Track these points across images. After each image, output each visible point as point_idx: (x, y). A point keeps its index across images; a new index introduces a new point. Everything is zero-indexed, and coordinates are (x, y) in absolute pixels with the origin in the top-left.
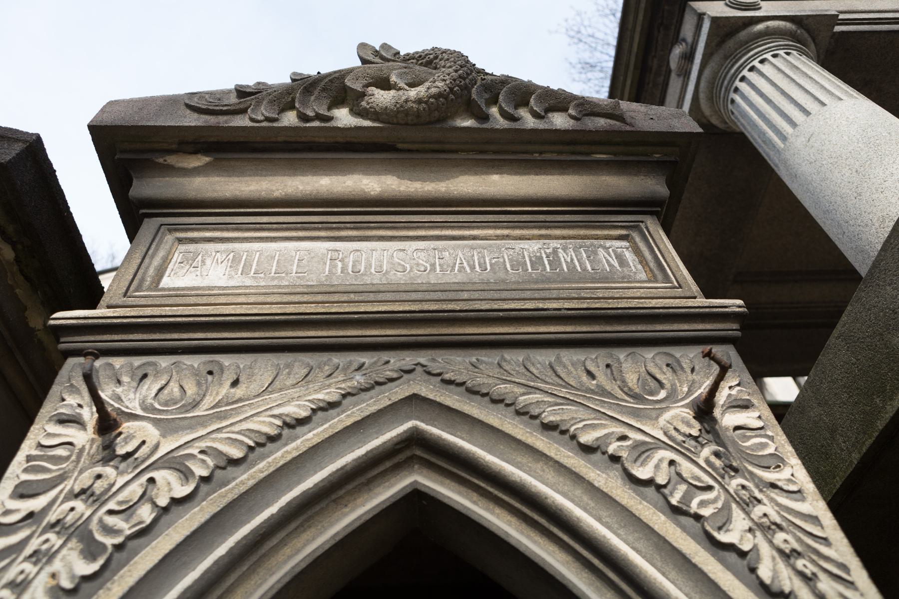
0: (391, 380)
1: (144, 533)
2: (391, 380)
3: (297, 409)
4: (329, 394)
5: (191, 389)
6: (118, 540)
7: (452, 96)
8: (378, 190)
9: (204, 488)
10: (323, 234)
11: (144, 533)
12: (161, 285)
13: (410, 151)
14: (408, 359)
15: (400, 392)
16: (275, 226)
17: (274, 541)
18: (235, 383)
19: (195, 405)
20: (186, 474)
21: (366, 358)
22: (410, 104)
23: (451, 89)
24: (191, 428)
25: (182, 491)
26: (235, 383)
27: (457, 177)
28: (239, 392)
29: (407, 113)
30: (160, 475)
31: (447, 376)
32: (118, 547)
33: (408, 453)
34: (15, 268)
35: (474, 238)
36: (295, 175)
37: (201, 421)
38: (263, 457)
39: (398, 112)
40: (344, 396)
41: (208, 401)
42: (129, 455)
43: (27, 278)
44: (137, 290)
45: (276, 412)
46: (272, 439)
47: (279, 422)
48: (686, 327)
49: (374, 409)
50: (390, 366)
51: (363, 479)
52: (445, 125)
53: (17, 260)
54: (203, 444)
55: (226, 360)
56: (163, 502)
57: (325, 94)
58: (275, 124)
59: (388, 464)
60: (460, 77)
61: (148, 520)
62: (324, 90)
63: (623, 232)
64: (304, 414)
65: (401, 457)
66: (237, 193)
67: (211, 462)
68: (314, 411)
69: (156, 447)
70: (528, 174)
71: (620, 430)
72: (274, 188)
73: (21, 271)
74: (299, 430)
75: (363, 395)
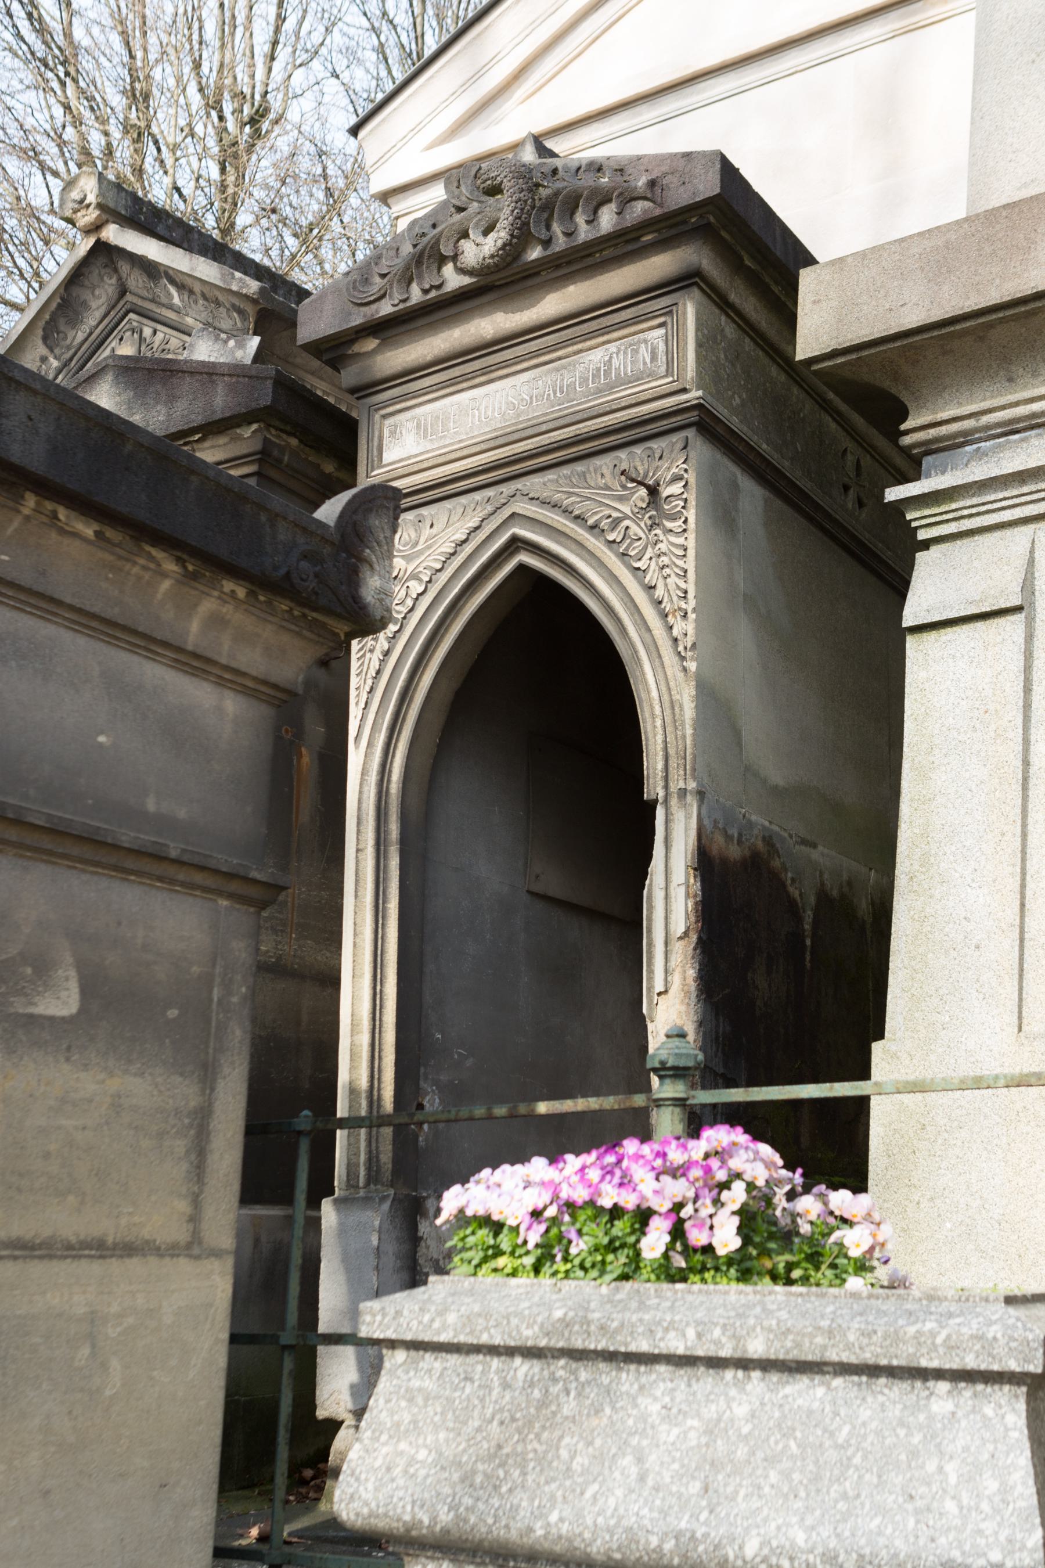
0: (504, 504)
1: (411, 610)
2: (504, 504)
3: (461, 536)
4: (473, 523)
5: (413, 535)
6: (403, 615)
7: (515, 240)
8: (492, 332)
9: (429, 585)
10: (465, 385)
11: (411, 610)
12: (384, 462)
13: (507, 284)
14: (507, 489)
15: (506, 512)
16: (434, 388)
17: (462, 602)
18: (432, 526)
19: (417, 543)
20: (420, 580)
21: (490, 492)
22: (488, 261)
23: (512, 235)
24: (418, 556)
25: (421, 589)
26: (432, 526)
27: (544, 298)
28: (434, 531)
29: (488, 266)
30: (411, 583)
31: (530, 496)
32: (404, 618)
33: (515, 546)
34: (302, 446)
35: (560, 359)
36: (436, 334)
37: (421, 552)
38: (450, 564)
39: (482, 269)
40: (482, 521)
41: (422, 540)
42: (396, 577)
43: (310, 447)
44: (372, 471)
45: (452, 539)
46: (453, 554)
47: (454, 545)
48: (665, 422)
49: (495, 527)
50: (503, 495)
51: (495, 565)
52: (520, 263)
53: (301, 441)
54: (424, 565)
55: (424, 511)
56: (415, 596)
57: (432, 260)
58: (408, 304)
59: (506, 554)
60: (516, 218)
61: (411, 605)
62: (429, 257)
63: (661, 320)
64: (464, 537)
65: (512, 549)
66: (405, 365)
67: (429, 573)
68: (469, 534)
69: (406, 570)
70: (595, 276)
71: (607, 512)
72: (426, 352)
73: (306, 445)
74: (464, 545)
75: (492, 517)
